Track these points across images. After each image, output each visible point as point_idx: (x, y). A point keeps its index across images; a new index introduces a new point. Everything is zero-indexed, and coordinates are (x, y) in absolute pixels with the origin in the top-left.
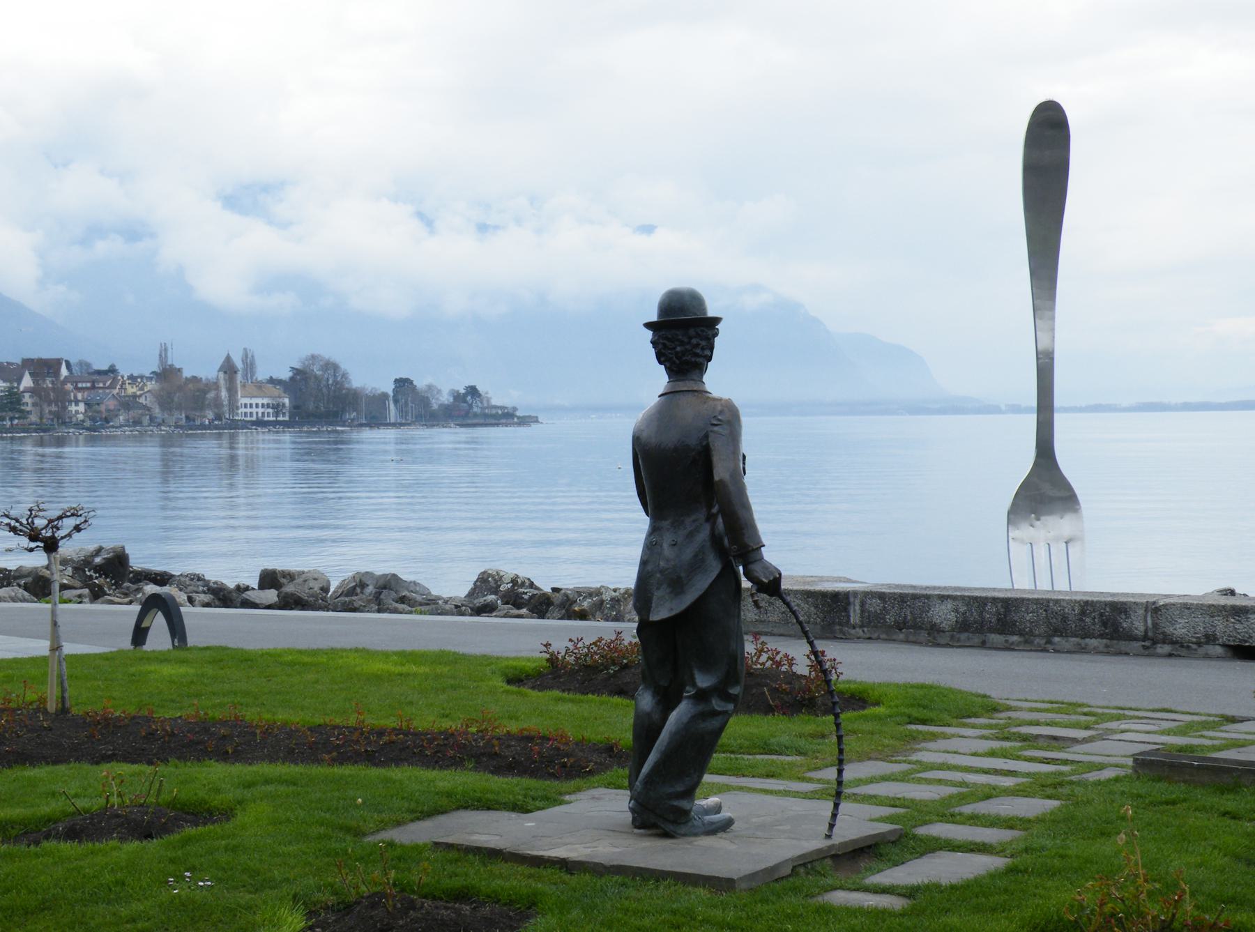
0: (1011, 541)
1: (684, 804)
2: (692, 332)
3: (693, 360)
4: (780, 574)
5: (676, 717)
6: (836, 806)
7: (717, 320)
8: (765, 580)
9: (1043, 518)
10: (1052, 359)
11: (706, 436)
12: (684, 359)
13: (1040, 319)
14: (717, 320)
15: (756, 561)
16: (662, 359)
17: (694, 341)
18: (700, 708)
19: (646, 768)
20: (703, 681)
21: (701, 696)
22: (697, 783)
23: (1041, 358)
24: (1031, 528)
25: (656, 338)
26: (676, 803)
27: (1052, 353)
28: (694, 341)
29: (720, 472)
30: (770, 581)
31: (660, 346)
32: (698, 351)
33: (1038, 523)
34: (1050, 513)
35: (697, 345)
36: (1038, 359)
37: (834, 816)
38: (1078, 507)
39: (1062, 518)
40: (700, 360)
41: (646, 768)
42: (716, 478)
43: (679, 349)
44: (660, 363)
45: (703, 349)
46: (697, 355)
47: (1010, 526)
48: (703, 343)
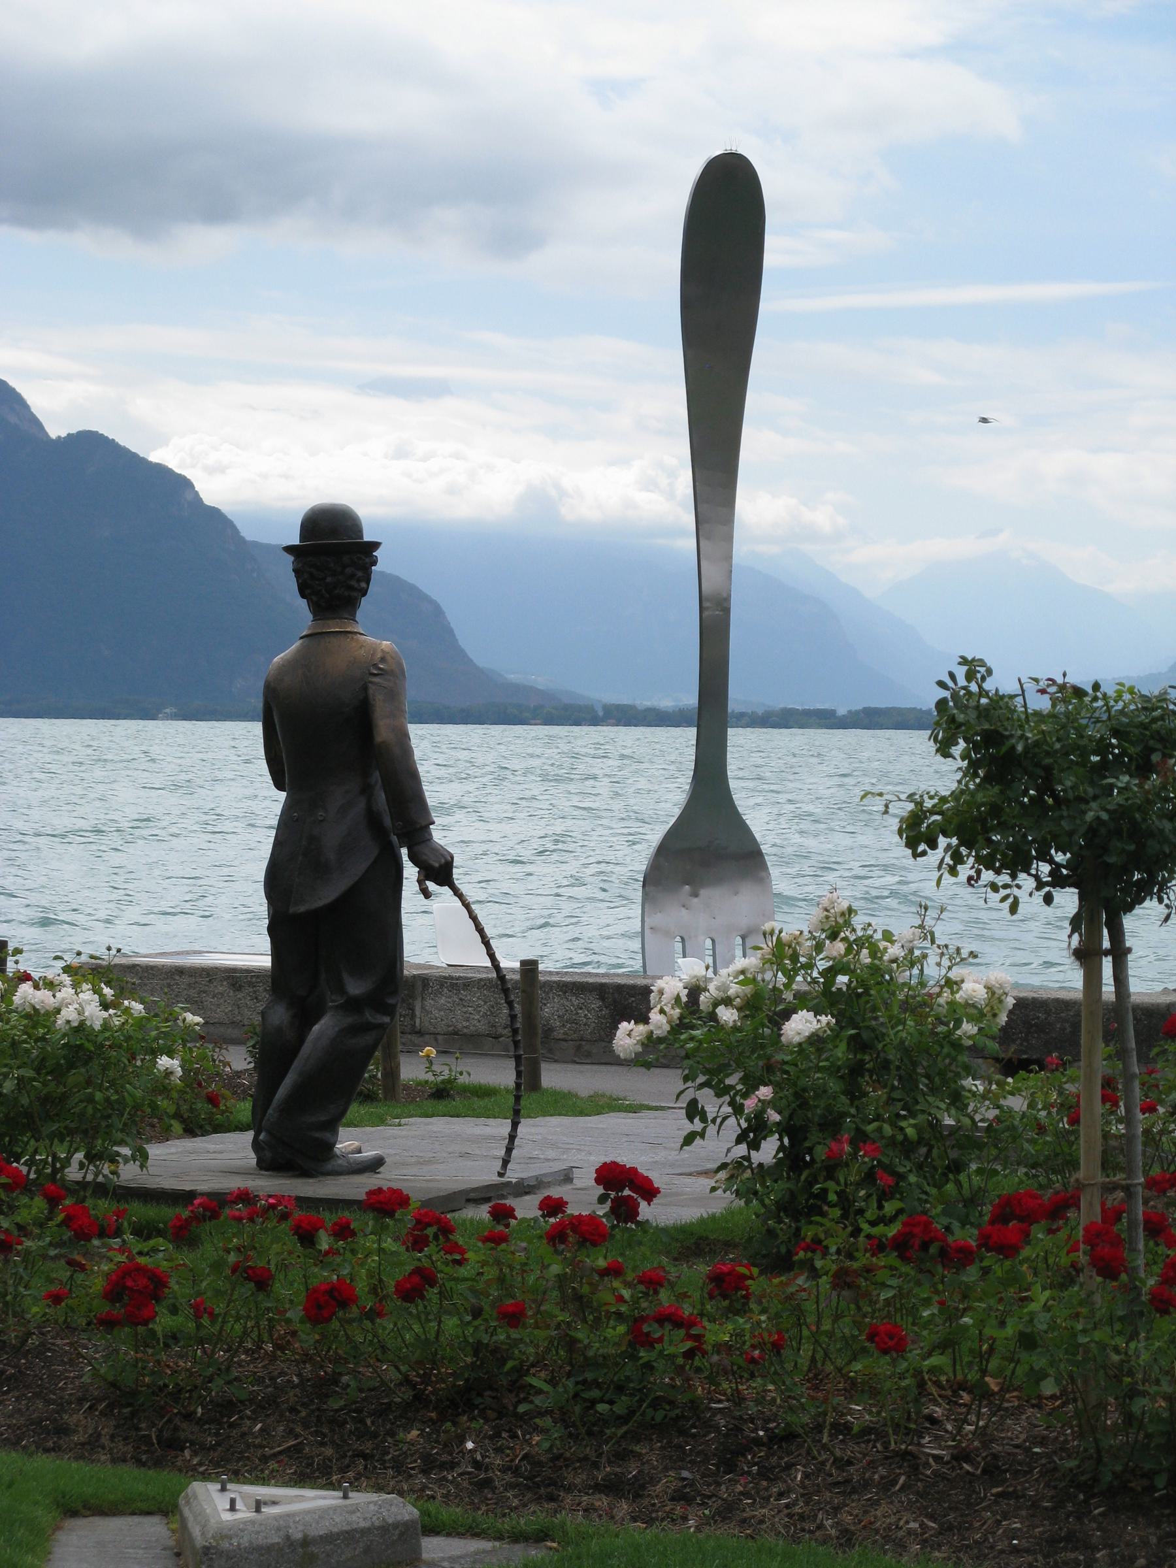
0: (647, 931)
1: (326, 1135)
2: (346, 559)
3: (346, 593)
4: (452, 858)
5: (323, 1028)
6: (515, 1125)
7: (375, 545)
8: (437, 865)
9: (703, 892)
10: (727, 611)
11: (365, 688)
12: (336, 592)
13: (708, 538)
14: (375, 545)
15: (423, 842)
16: (308, 592)
17: (349, 571)
18: (349, 1020)
19: (282, 1091)
20: (356, 988)
21: (353, 1005)
22: (343, 1113)
23: (708, 608)
24: (683, 909)
25: (300, 565)
26: (317, 1135)
27: (728, 599)
28: (349, 571)
29: (383, 732)
30: (441, 866)
31: (306, 576)
32: (353, 583)
33: (695, 900)
34: (718, 881)
35: (352, 576)
36: (702, 609)
37: (512, 1137)
38: (763, 874)
39: (736, 893)
40: (355, 594)
41: (282, 1091)
42: (378, 739)
43: (329, 580)
44: (303, 595)
45: (359, 581)
46: (351, 588)
47: (646, 906)
48: (360, 574)
